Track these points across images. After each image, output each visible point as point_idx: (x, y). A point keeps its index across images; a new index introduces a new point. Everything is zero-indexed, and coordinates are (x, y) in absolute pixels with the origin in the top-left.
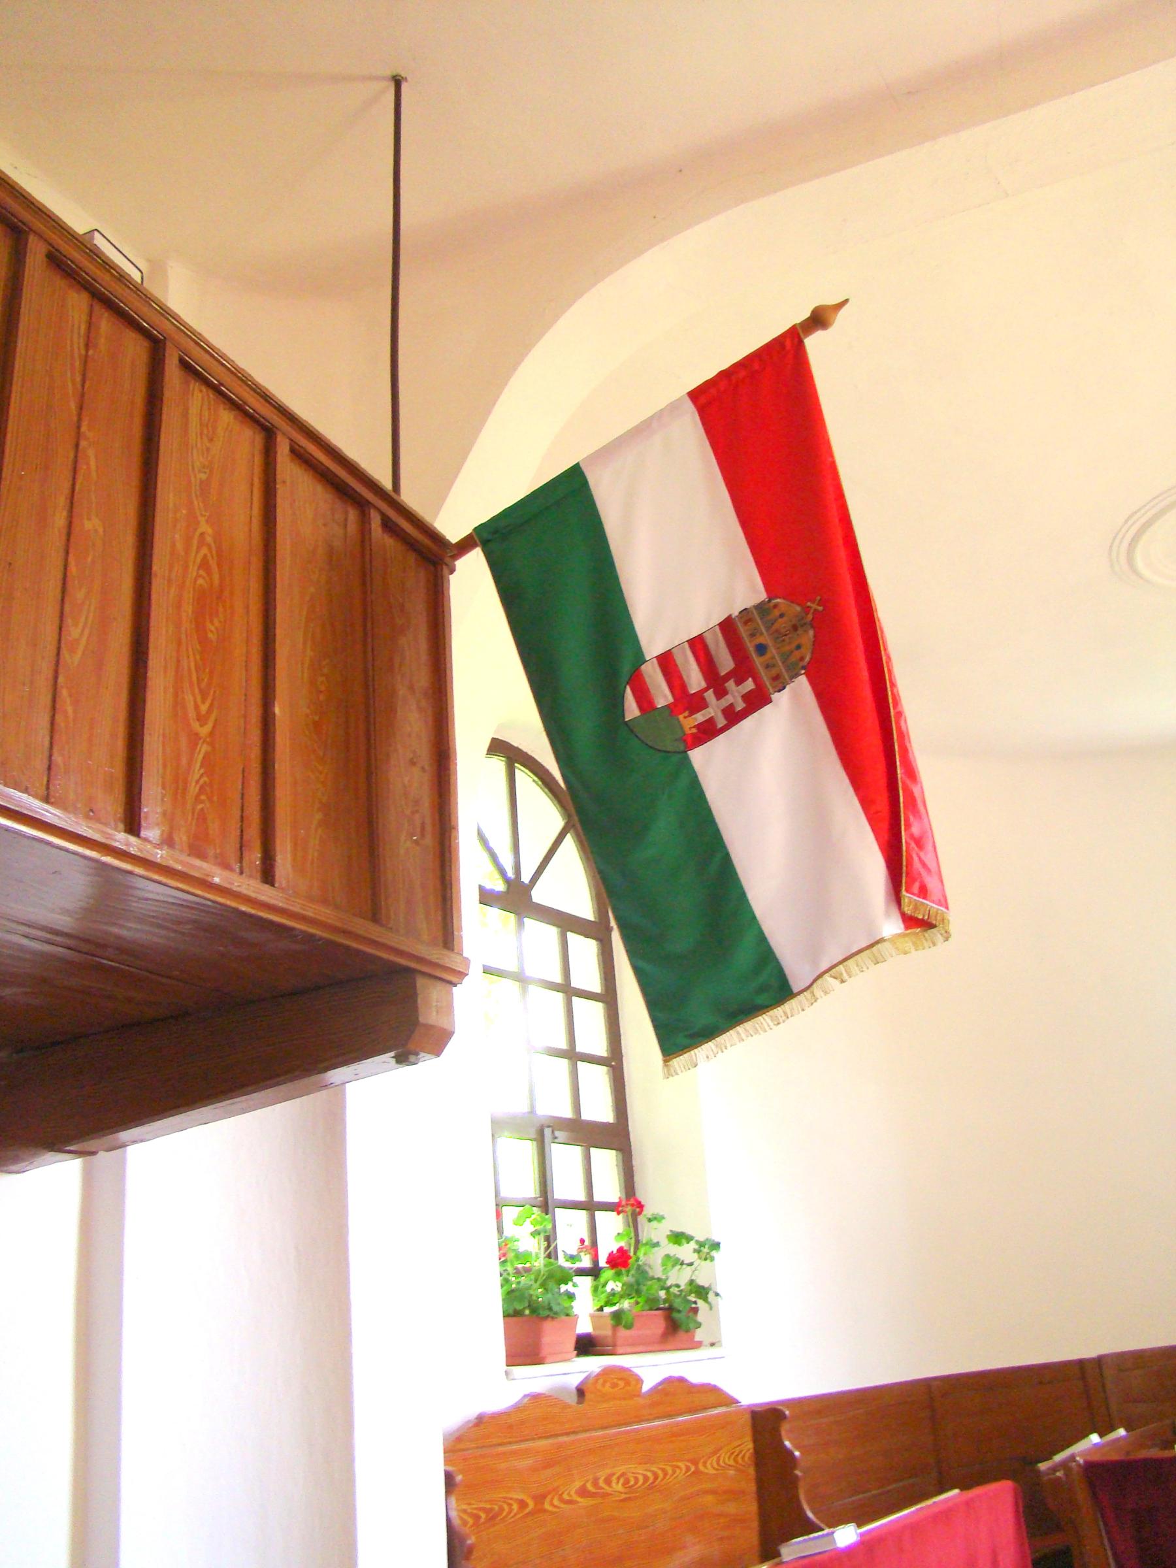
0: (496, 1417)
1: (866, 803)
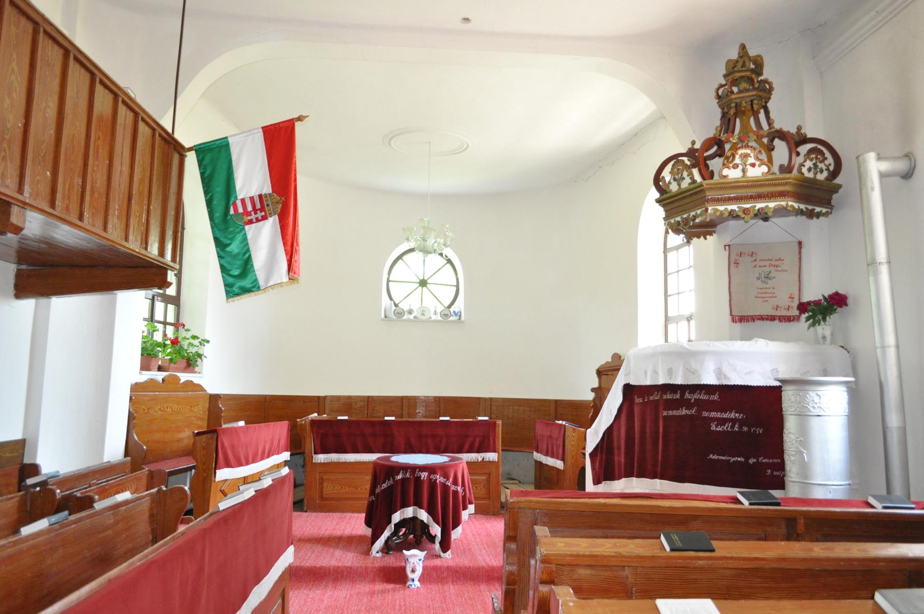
0: (141, 383)
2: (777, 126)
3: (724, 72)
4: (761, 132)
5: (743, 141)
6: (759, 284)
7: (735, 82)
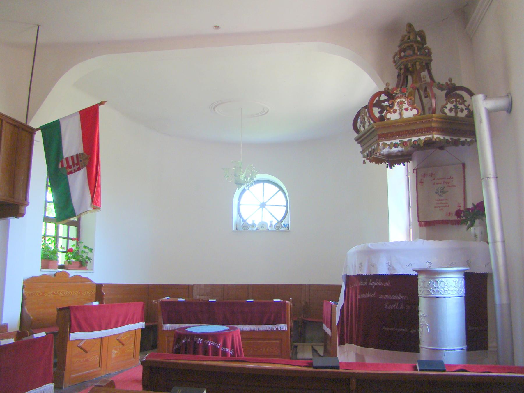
0: (36, 277)
1: (90, 189)
7: (404, 50)
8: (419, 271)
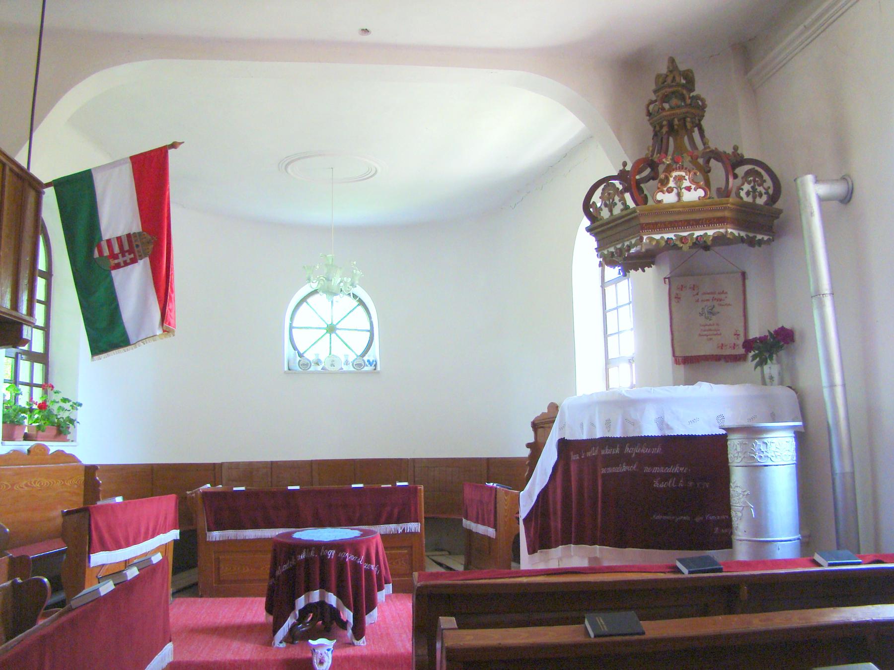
1: (158, 297)
2: (712, 145)
3: (653, 87)
4: (696, 153)
5: (677, 164)
6: (702, 320)
7: (665, 98)
8: (729, 430)
